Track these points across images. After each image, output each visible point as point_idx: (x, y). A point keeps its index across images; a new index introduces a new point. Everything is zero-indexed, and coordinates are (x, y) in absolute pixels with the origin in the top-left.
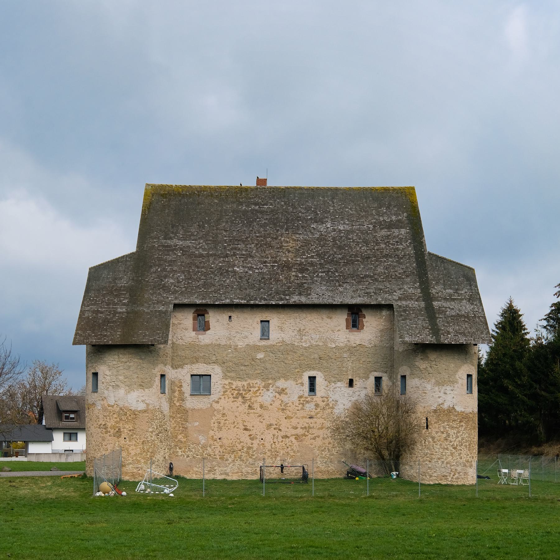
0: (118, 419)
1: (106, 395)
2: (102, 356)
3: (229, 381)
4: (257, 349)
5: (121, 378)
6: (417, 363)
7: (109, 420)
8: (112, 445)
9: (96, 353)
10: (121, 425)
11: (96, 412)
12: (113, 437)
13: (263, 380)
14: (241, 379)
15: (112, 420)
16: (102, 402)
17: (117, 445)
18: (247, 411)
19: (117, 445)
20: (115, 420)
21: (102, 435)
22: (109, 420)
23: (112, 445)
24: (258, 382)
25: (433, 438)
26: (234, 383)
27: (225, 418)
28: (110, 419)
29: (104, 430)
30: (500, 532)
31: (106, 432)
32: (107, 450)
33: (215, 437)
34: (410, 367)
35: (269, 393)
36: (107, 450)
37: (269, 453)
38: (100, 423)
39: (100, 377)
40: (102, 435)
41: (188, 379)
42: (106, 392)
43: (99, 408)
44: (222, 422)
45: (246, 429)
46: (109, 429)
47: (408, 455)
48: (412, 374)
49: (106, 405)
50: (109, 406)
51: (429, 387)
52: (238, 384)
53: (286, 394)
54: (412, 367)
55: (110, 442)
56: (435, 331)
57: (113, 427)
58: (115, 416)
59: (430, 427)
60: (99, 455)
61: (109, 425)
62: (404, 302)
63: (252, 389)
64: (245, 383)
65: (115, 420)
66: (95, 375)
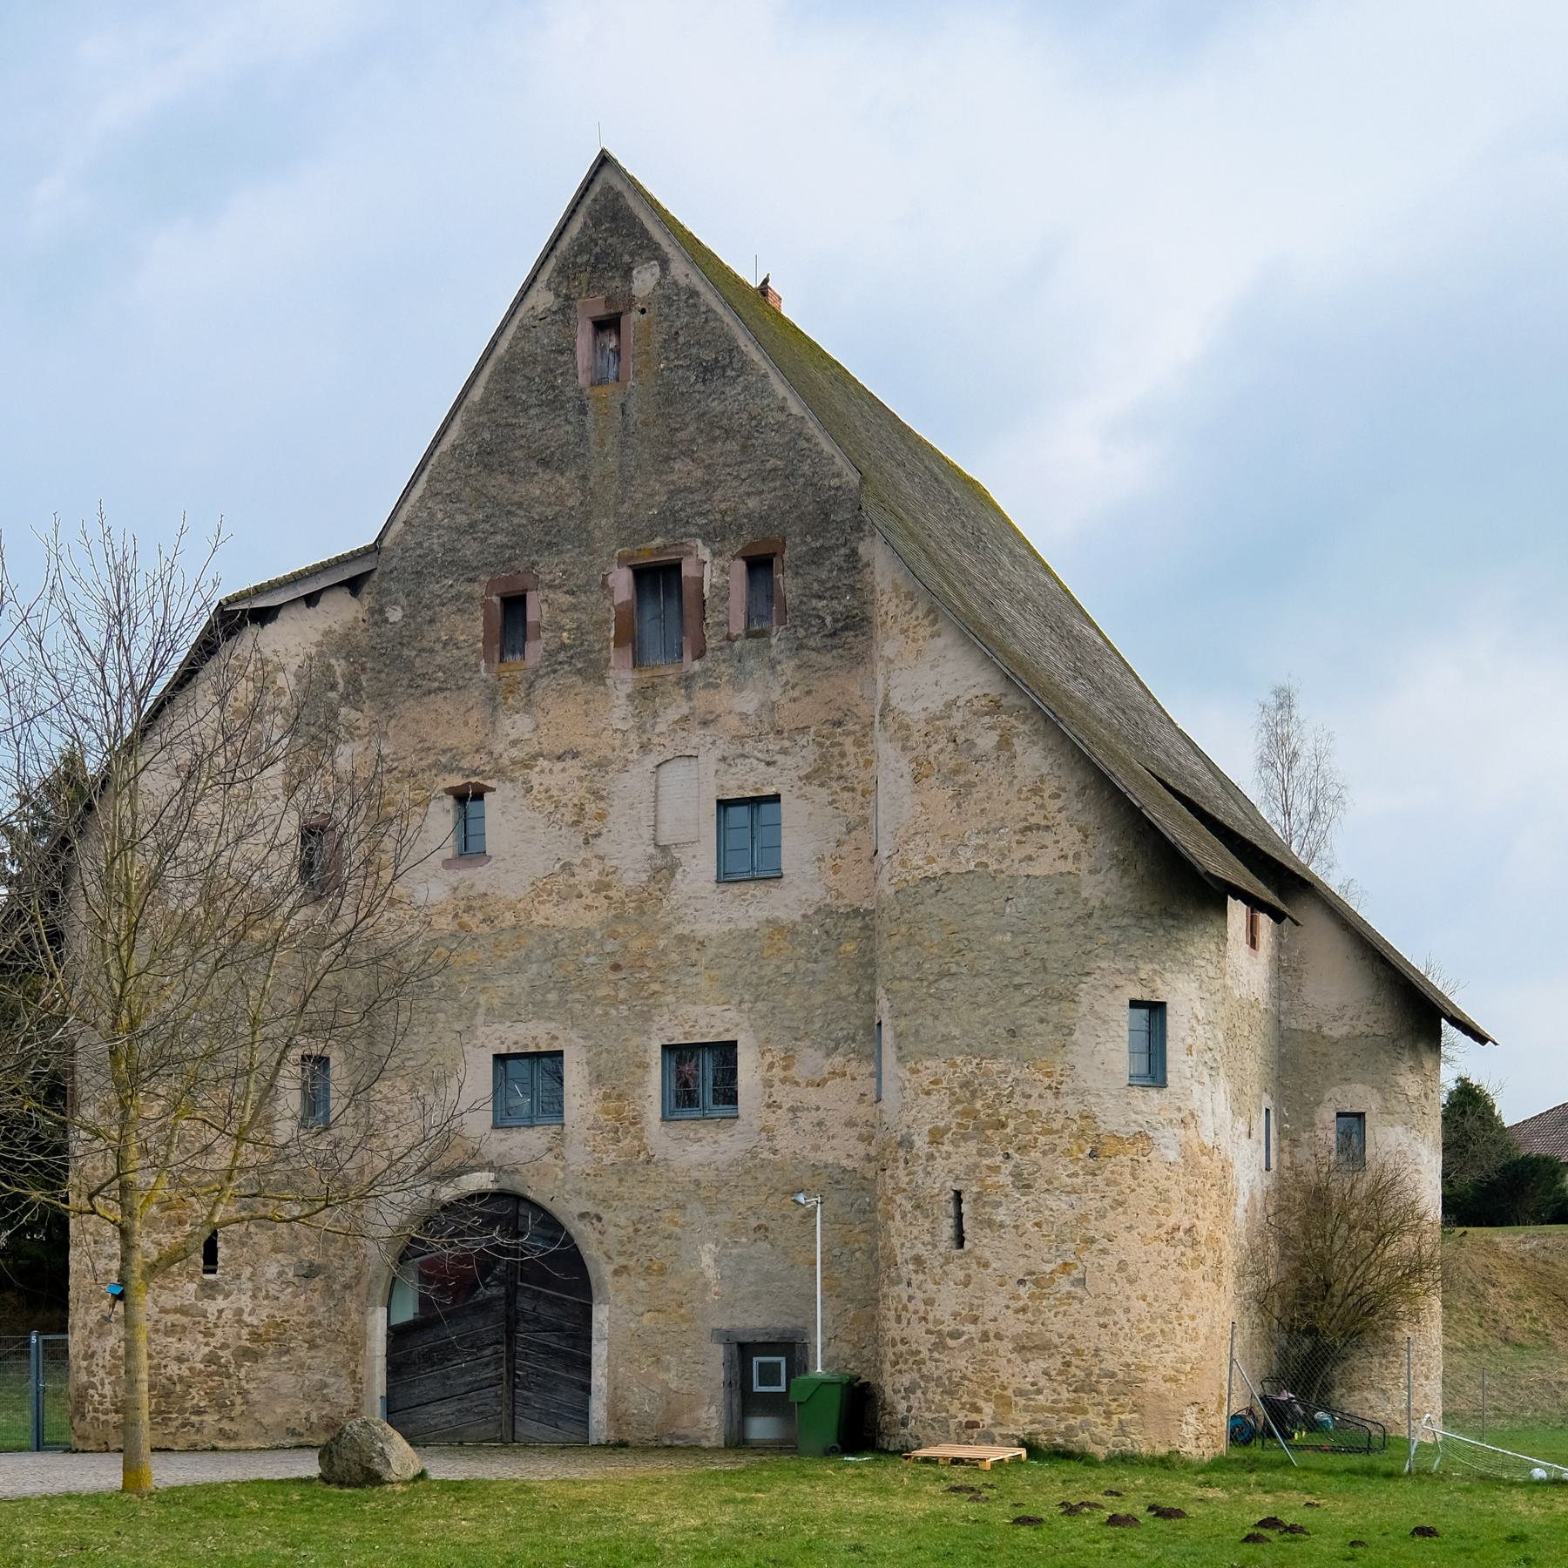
1: (1193, 1104)
2: (1181, 935)
6: (1401, 1080)
8: (1207, 1315)
9: (1150, 916)
11: (1154, 1171)
16: (1180, 1132)
21: (1183, 1275)
29: (1190, 1253)
30: (739, 1495)
34: (1380, 1090)
38: (1171, 1222)
39: (1176, 1025)
40: (1183, 1275)
41: (657, 1054)
43: (1172, 1155)
47: (1376, 1360)
54: (1386, 1088)
56: (235, 983)
60: (1169, 1359)
66: (1156, 1009)
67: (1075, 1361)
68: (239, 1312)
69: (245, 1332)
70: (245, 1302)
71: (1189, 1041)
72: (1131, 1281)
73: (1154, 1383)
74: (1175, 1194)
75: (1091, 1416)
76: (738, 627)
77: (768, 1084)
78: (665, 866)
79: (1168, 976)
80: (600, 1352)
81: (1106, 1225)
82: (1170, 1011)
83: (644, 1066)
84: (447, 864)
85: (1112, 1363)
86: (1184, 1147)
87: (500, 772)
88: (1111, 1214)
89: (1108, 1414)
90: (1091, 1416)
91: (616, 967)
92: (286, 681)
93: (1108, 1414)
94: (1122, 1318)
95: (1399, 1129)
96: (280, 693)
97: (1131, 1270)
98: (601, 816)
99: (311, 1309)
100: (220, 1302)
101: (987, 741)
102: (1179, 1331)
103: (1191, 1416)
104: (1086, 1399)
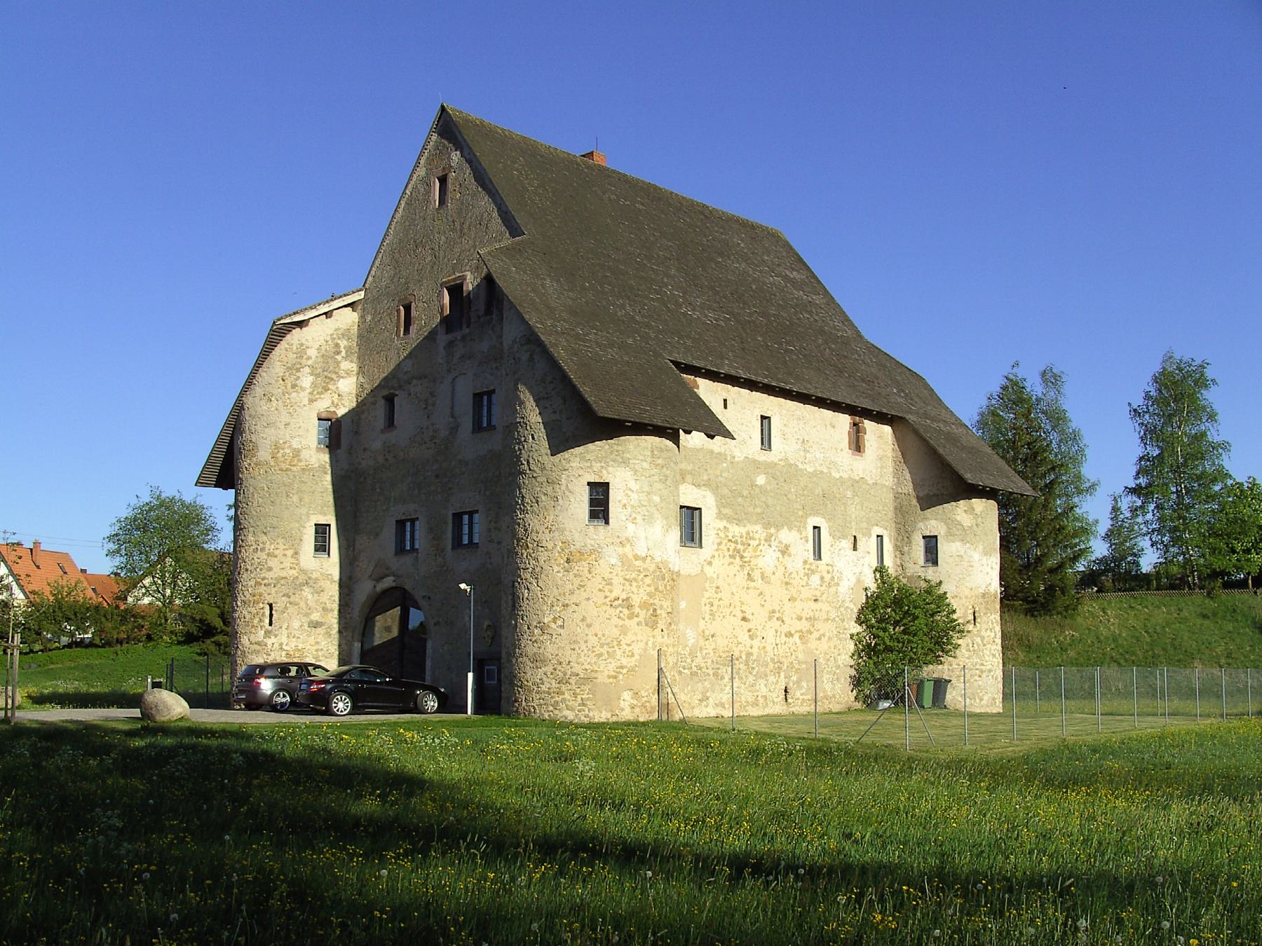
0: (652, 589)
3: (724, 523)
4: (757, 466)
5: (656, 499)
7: (635, 590)
10: (656, 601)
11: (602, 569)
12: (644, 627)
13: (767, 526)
14: (739, 522)
15: (641, 590)
16: (620, 550)
17: (650, 644)
18: (745, 584)
19: (650, 644)
20: (648, 589)
22: (635, 590)
23: (642, 645)
24: (758, 530)
25: (983, 638)
26: (731, 529)
27: (719, 596)
28: (638, 587)
29: (626, 611)
31: (631, 617)
32: (633, 655)
33: (707, 633)
35: (771, 551)
36: (633, 655)
37: (771, 666)
40: (621, 623)
41: (450, 517)
42: (631, 527)
43: (613, 561)
44: (716, 603)
45: (744, 619)
46: (637, 610)
48: (950, 534)
49: (630, 556)
50: (637, 557)
51: (976, 556)
52: (736, 530)
53: (790, 555)
55: (639, 638)
57: (644, 605)
58: (648, 581)
59: (978, 620)
61: (636, 600)
62: (1044, 419)
63: (751, 542)
64: (743, 530)
65: (648, 589)
67: (559, 667)
68: (281, 644)
69: (284, 653)
70: (284, 640)
71: (625, 501)
72: (589, 626)
73: (602, 678)
74: (616, 581)
75: (567, 696)
76: (482, 312)
77: (489, 530)
78: (454, 429)
79: (610, 469)
80: (428, 663)
81: (574, 599)
82: (611, 487)
83: (446, 523)
84: (382, 431)
85: (577, 669)
86: (623, 559)
87: (400, 387)
88: (577, 592)
89: (575, 695)
90: (567, 696)
91: (437, 476)
92: (312, 352)
93: (575, 695)
94: (583, 647)
95: (958, 544)
96: (309, 358)
97: (589, 621)
98: (433, 405)
99: (317, 643)
100: (273, 640)
101: (525, 357)
102: (619, 652)
103: (627, 695)
104: (564, 688)
